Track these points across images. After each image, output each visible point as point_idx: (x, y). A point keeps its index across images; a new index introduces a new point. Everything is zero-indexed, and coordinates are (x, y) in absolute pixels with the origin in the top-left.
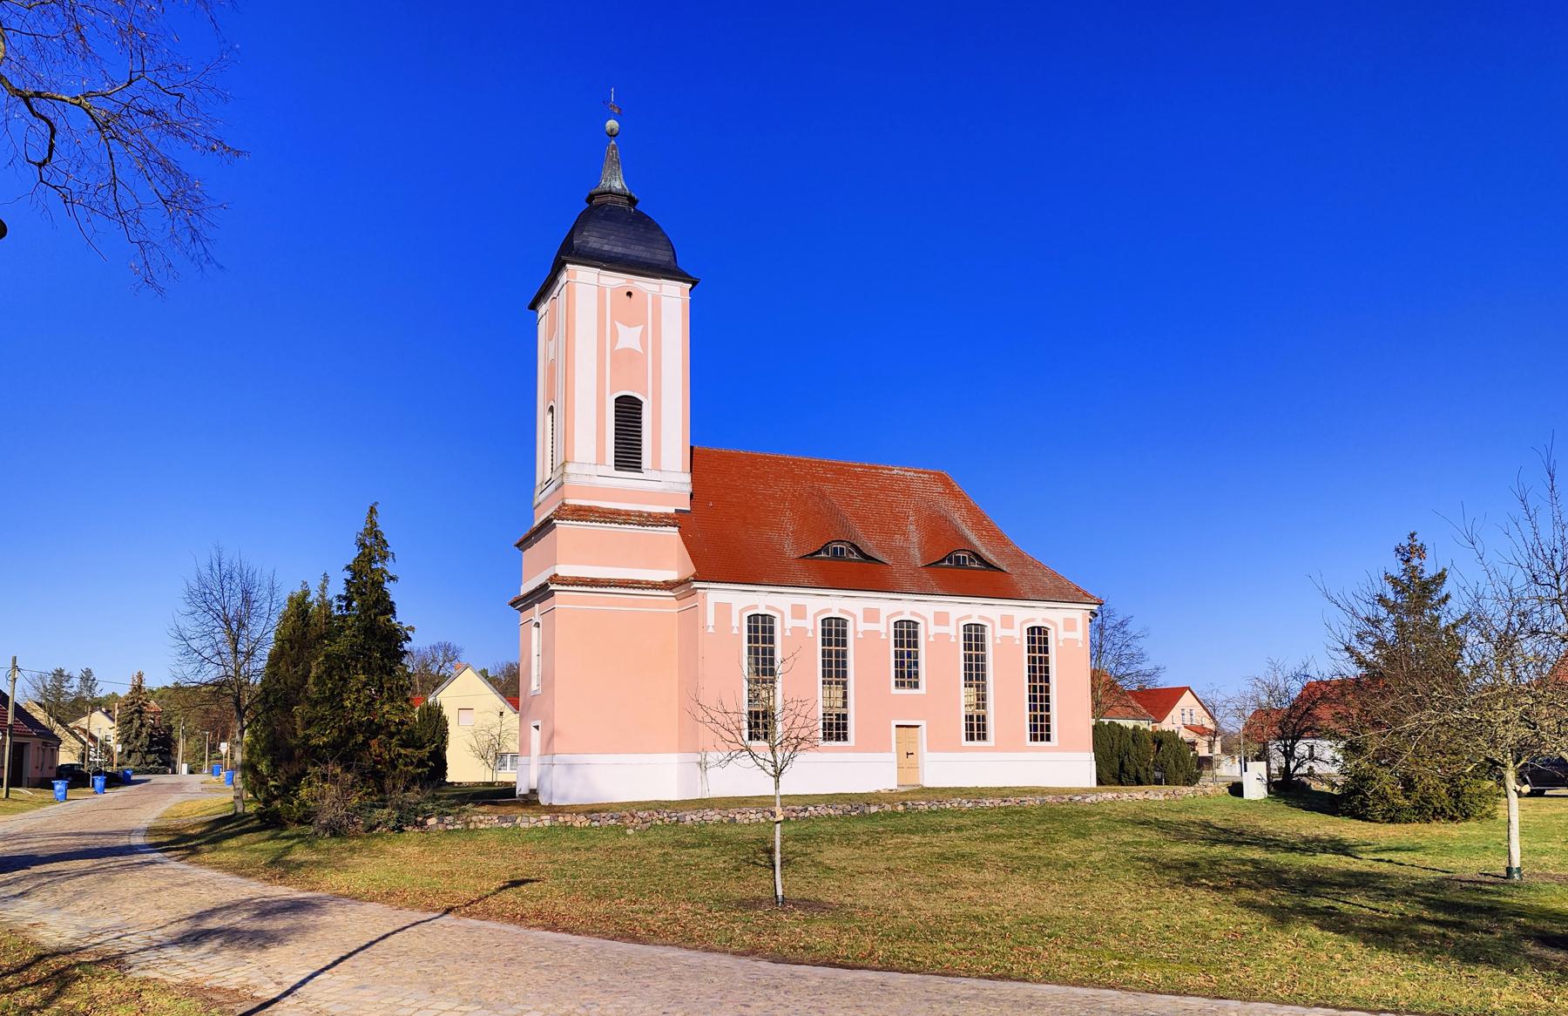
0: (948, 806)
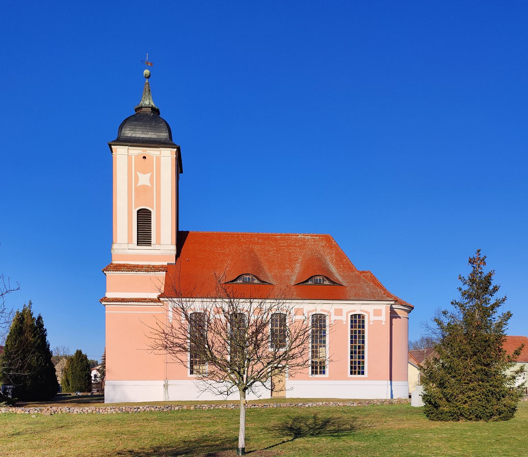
0: (220, 407)
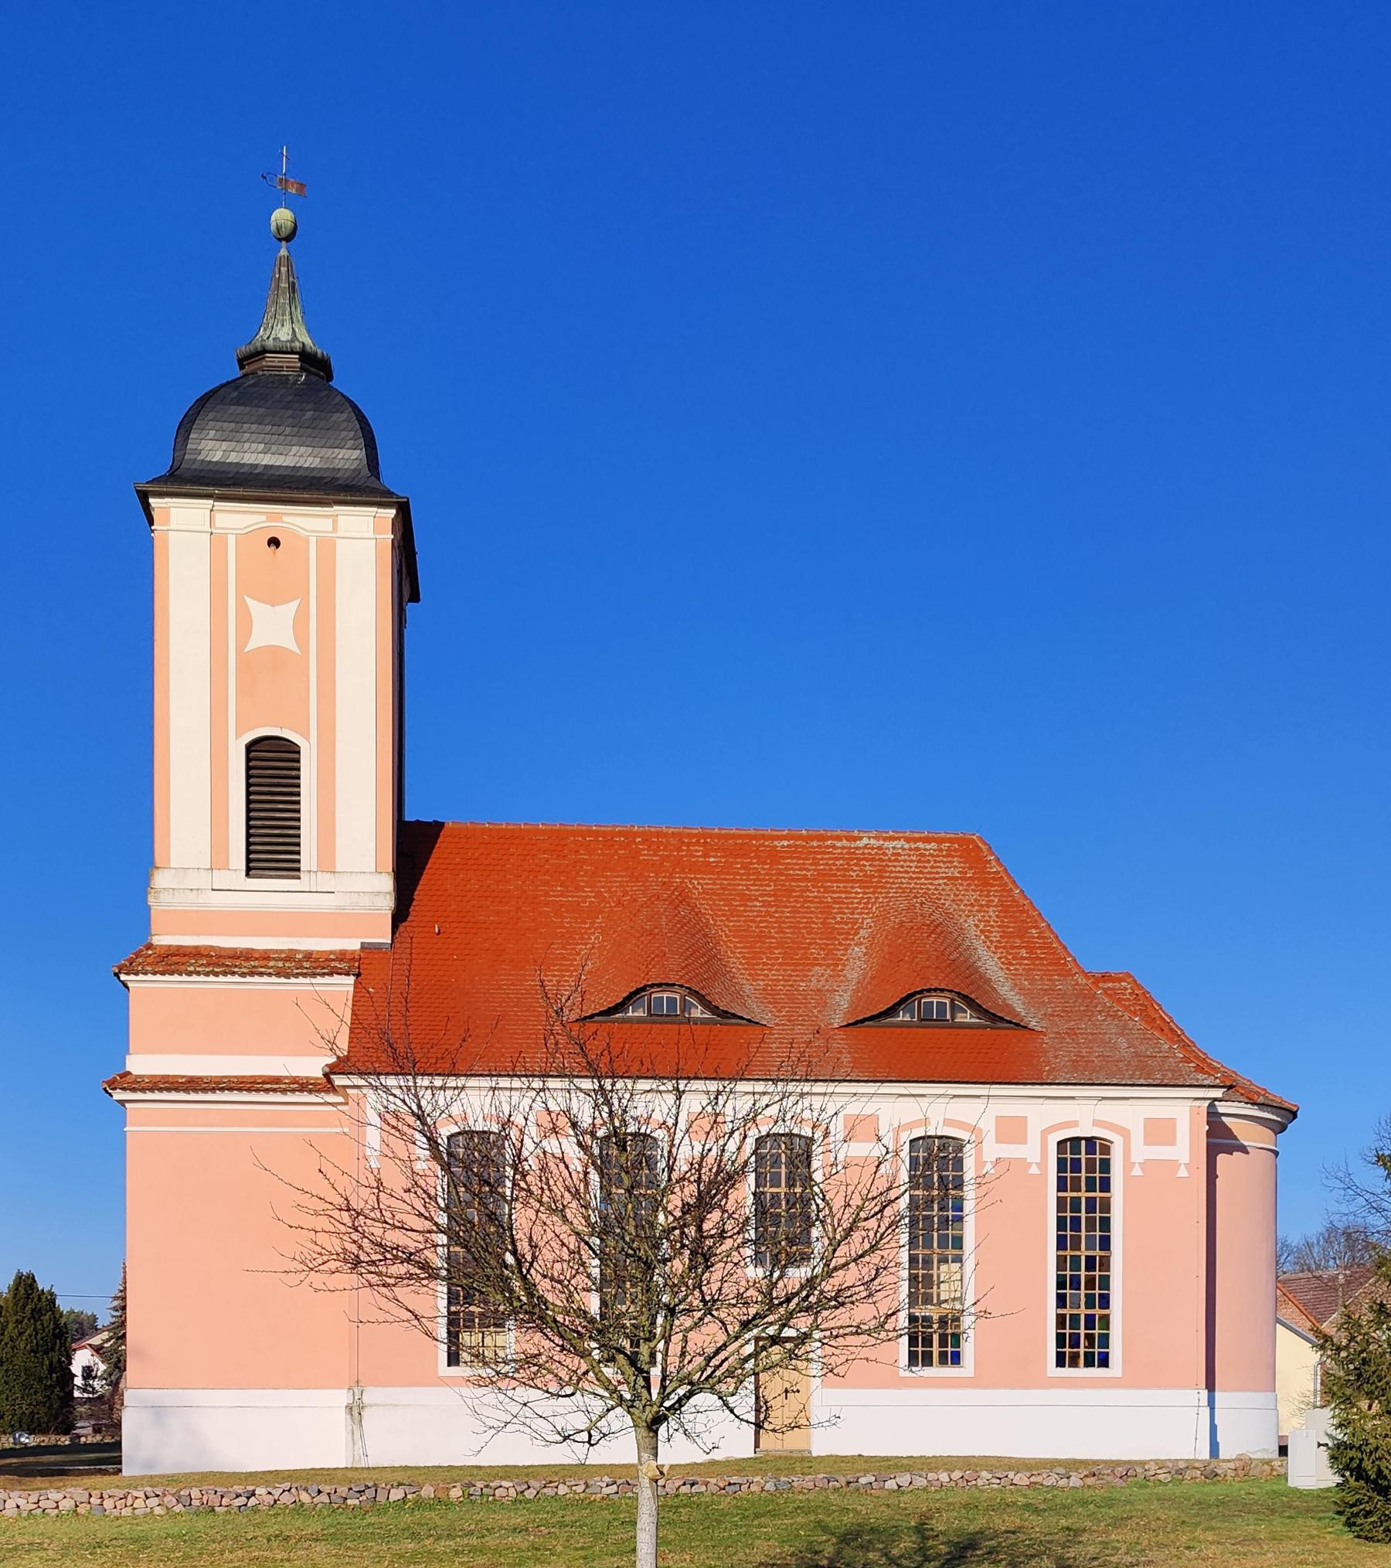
0: (562, 1490)
